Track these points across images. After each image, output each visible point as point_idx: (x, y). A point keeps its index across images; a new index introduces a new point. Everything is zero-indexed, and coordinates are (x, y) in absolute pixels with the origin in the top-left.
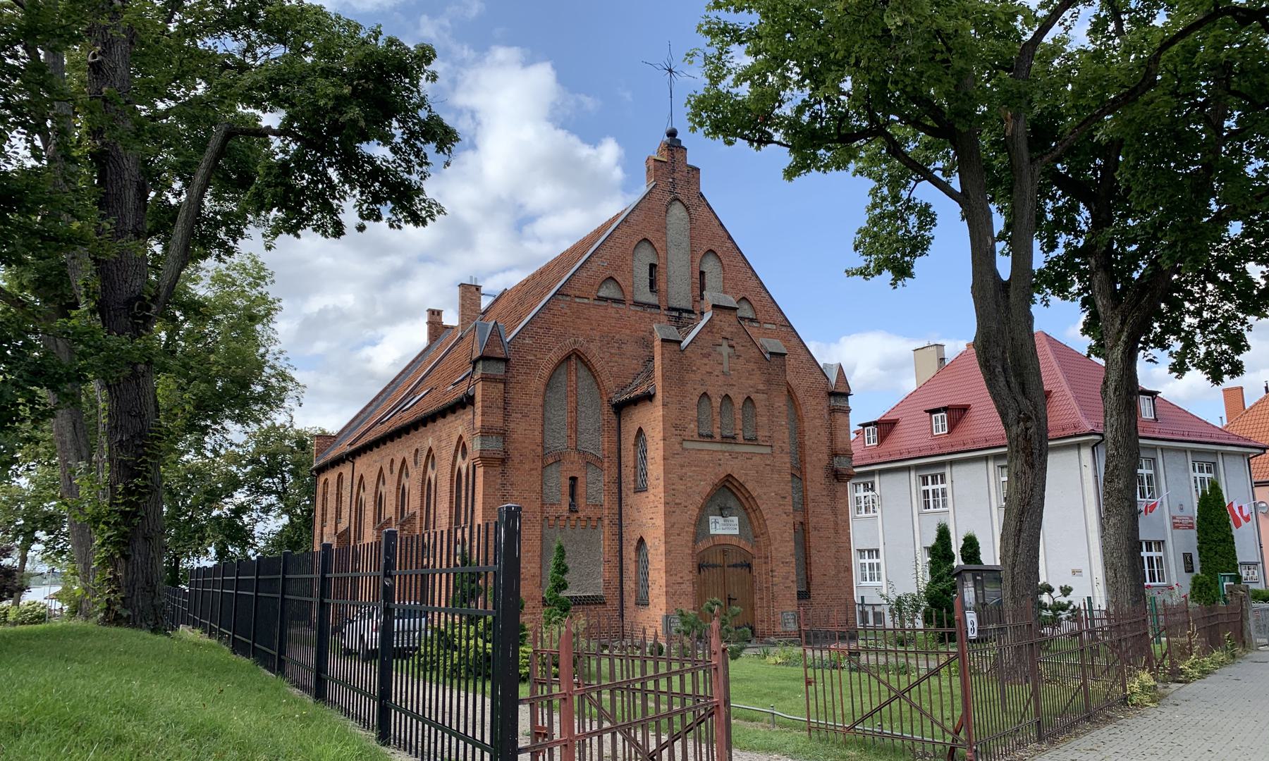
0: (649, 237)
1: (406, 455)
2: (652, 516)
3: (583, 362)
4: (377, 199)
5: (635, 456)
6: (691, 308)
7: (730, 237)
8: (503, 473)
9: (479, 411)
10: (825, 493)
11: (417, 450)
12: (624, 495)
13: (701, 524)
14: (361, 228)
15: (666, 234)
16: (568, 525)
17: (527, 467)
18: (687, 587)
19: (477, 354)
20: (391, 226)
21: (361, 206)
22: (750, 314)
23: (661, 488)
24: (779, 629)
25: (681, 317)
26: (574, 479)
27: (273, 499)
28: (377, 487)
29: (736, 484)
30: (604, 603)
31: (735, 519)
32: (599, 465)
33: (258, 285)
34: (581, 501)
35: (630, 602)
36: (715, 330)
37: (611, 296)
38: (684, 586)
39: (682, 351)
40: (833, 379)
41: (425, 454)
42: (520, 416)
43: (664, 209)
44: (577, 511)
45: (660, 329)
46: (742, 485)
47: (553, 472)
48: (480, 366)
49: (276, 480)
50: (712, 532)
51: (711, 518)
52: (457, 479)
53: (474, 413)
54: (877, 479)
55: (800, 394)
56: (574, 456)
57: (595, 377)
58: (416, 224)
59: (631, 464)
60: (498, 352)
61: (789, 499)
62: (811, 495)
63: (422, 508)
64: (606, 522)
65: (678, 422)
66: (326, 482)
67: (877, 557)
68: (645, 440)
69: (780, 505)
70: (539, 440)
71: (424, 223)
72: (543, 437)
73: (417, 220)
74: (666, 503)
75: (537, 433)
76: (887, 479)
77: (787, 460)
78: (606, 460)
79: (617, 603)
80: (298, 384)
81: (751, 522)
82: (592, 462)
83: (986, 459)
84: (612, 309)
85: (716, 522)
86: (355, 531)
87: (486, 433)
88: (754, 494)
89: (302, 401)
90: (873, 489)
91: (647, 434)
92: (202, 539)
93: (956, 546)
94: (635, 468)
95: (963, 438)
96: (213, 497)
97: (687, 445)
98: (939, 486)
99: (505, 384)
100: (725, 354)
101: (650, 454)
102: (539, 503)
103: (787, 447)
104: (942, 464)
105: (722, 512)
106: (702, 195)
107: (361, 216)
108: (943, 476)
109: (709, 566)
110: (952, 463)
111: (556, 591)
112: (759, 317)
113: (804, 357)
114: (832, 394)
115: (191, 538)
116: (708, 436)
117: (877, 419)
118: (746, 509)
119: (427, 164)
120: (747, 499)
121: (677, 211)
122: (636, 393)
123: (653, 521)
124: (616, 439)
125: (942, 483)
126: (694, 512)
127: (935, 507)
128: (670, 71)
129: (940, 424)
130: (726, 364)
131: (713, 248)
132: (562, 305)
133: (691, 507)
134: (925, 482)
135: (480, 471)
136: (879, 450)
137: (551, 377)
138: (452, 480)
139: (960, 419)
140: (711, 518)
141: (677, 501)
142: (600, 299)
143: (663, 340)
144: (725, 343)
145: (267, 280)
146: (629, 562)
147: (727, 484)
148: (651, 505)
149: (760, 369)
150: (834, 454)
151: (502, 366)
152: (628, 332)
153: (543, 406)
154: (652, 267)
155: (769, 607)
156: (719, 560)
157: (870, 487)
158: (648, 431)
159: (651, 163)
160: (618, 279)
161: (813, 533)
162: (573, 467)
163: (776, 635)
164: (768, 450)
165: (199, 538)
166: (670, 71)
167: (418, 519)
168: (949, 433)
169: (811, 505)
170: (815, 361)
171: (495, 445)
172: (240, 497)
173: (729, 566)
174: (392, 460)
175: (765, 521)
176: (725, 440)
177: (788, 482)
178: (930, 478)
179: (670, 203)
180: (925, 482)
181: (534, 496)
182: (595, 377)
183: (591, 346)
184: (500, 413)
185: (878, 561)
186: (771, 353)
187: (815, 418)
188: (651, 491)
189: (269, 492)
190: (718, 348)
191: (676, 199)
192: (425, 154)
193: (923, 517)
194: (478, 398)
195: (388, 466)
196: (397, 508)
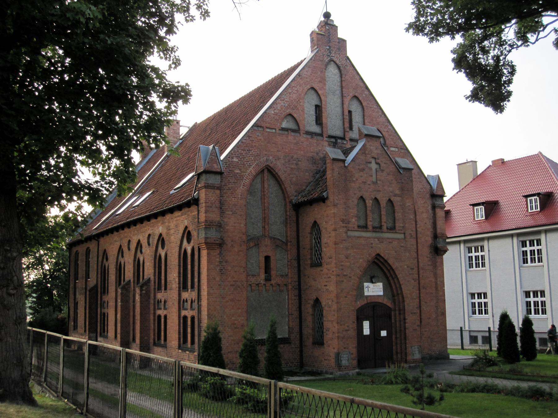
1: (141, 238)
2: (326, 284)
5: (311, 240)
8: (220, 253)
11: (149, 235)
12: (302, 268)
17: (236, 249)
26: (267, 259)
28: (117, 259)
34: (273, 273)
35: (309, 342)
36: (367, 152)
38: (349, 332)
40: (434, 186)
41: (157, 238)
42: (231, 213)
46: (386, 261)
48: (204, 177)
50: (366, 294)
53: (198, 211)
60: (216, 168)
63: (155, 276)
65: (344, 218)
75: (242, 225)
79: (298, 342)
83: (512, 236)
84: (291, 137)
85: (368, 287)
88: (394, 267)
94: (311, 249)
97: (350, 233)
98: (480, 254)
100: (374, 169)
105: (372, 280)
108: (482, 247)
110: (489, 239)
120: (389, 270)
123: (327, 287)
130: (374, 176)
131: (356, 95)
132: (258, 134)
134: (470, 251)
135: (204, 253)
141: (345, 273)
142: (283, 129)
148: (325, 276)
151: (218, 177)
154: (317, 107)
158: (323, 225)
162: (267, 249)
164: (402, 236)
167: (152, 283)
188: (325, 266)
190: (369, 165)
195: (126, 244)
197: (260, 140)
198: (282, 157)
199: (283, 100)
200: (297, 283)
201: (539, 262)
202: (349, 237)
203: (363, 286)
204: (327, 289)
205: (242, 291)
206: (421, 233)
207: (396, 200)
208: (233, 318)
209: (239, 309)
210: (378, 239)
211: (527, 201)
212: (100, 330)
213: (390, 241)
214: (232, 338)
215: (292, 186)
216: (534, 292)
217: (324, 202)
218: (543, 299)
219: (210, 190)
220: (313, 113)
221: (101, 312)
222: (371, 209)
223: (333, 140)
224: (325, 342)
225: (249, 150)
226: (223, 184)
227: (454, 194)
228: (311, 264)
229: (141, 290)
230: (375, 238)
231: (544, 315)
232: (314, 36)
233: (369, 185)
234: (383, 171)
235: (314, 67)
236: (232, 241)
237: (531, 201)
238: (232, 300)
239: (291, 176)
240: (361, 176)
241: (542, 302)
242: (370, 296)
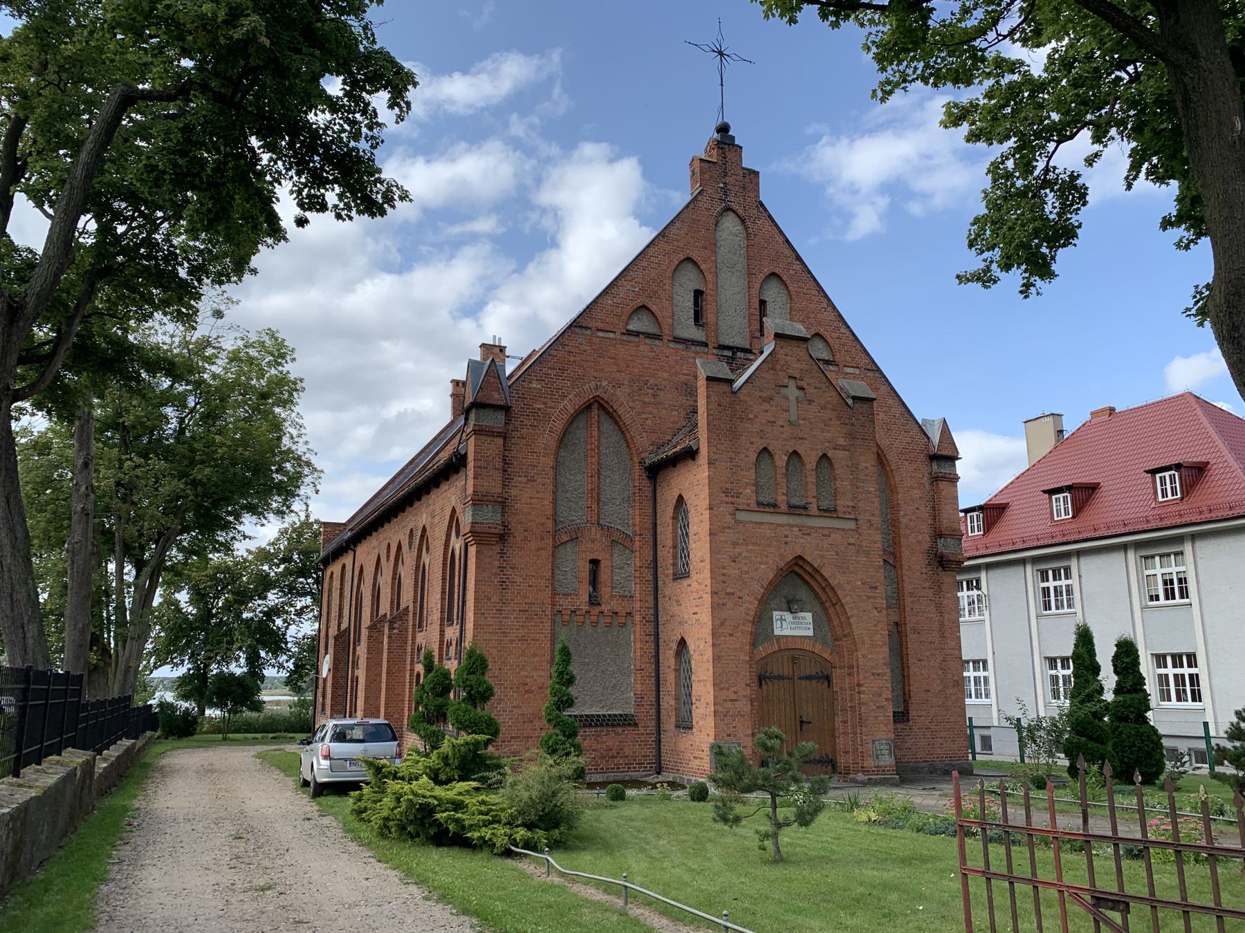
0: (694, 256)
2: (696, 610)
3: (608, 413)
4: (318, 180)
6: (748, 347)
7: (799, 258)
8: (502, 553)
9: (471, 473)
10: (927, 585)
11: (411, 530)
12: (660, 584)
13: (761, 621)
14: (301, 222)
15: (716, 252)
16: (588, 622)
18: (744, 706)
19: (469, 400)
20: (339, 216)
21: (300, 192)
22: (826, 355)
23: (707, 573)
24: (869, 763)
25: (735, 355)
26: (595, 562)
27: (308, 600)
29: (808, 568)
30: (636, 725)
31: (808, 616)
32: (628, 544)
33: (280, 364)
34: (605, 591)
35: (669, 723)
36: (778, 367)
37: (644, 329)
38: (738, 704)
39: (734, 393)
40: (935, 437)
42: (524, 480)
43: (713, 221)
44: (599, 604)
45: (703, 366)
47: (568, 552)
48: (472, 416)
49: (310, 581)
50: (777, 632)
51: (775, 613)
52: (449, 561)
54: (983, 575)
55: (892, 457)
56: (595, 533)
57: (623, 433)
58: (373, 215)
59: (669, 543)
60: (496, 398)
61: (881, 589)
62: (908, 587)
63: (415, 602)
64: (638, 618)
66: (332, 573)
67: (985, 669)
68: (686, 512)
69: (869, 598)
70: (549, 512)
71: (383, 213)
72: (555, 508)
73: (372, 208)
74: (714, 593)
75: (546, 502)
76: (996, 574)
77: (878, 537)
78: (637, 538)
80: (315, 470)
81: (829, 619)
82: (619, 541)
83: (1124, 547)
84: (645, 346)
86: (355, 631)
87: (478, 501)
88: (834, 583)
89: (319, 487)
90: (978, 588)
91: (688, 503)
92: (231, 643)
93: (1105, 654)
94: (675, 547)
95: (1092, 523)
96: (243, 597)
97: (742, 516)
98: (1063, 583)
99: (505, 438)
100: (792, 398)
101: (692, 529)
102: (549, 592)
103: (877, 520)
104: (1066, 555)
105: (791, 606)
106: (762, 205)
107: (301, 205)
108: (1068, 571)
109: (775, 677)
110: (1079, 554)
111: (559, 709)
112: (838, 358)
113: (898, 410)
114: (934, 458)
115: (219, 642)
116: (769, 505)
117: (982, 503)
118: (822, 603)
119: (379, 125)
121: (730, 224)
122: (675, 450)
123: (696, 617)
124: (650, 511)
125: (1067, 578)
126: (751, 605)
127: (1057, 608)
128: (721, 53)
129: (1062, 506)
130: (793, 410)
132: (580, 340)
133: (746, 598)
134: (1045, 578)
135: (472, 550)
136: (986, 540)
137: (566, 431)
138: (444, 564)
139: (1087, 500)
140: (775, 613)
141: (729, 590)
143: (709, 379)
144: (792, 384)
145: (288, 358)
146: (668, 670)
147: (797, 569)
148: (695, 595)
149: (839, 418)
150: (938, 535)
151: (501, 416)
152: (666, 375)
153: (555, 468)
154: (698, 294)
155: (855, 733)
156: (787, 671)
157: (975, 585)
159: (697, 164)
160: (654, 308)
161: (912, 637)
163: (864, 771)
164: (852, 525)
165: (228, 642)
166: (721, 53)
167: (411, 614)
168: (1073, 517)
169: (908, 600)
170: (911, 415)
171: (491, 517)
172: (273, 598)
173: (800, 678)
174: (389, 545)
175: (848, 618)
176: (792, 511)
177: (880, 567)
178: (1050, 573)
179: (721, 214)
180: (1045, 578)
181: (543, 583)
182: (623, 433)
183: (618, 392)
184: (498, 476)
185: (986, 674)
186: (854, 398)
187: (911, 487)
188: (694, 576)
189: (304, 594)
190: (783, 391)
191: (728, 209)
192: (374, 111)
193: (1043, 621)
194: (471, 457)
196: (392, 602)
197: (585, 351)
198: (626, 382)
199: (631, 281)
200: (652, 612)
201: (1182, 597)
202: (738, 522)
203: (772, 618)
204: (698, 620)
205: (542, 622)
206: (907, 527)
207: (837, 456)
208: (523, 673)
209: (535, 655)
210: (801, 528)
211: (1154, 482)
212: (351, 707)
213: (827, 532)
214: (520, 711)
215: (644, 434)
216: (1173, 656)
217: (693, 459)
218: (1193, 671)
219: (483, 437)
220: (691, 304)
221: (353, 676)
222: (784, 471)
223: (728, 353)
224: (694, 723)
225: (563, 370)
226: (511, 427)
227: (1017, 475)
228: (674, 574)
229: (391, 628)
230: (793, 526)
231: (1198, 703)
232: (697, 164)
233: (782, 426)
234: (810, 401)
235: (693, 220)
236: (526, 531)
237: (1163, 480)
238: (523, 639)
239: (643, 416)
240: (766, 411)
241: (1191, 676)
242: (786, 636)
